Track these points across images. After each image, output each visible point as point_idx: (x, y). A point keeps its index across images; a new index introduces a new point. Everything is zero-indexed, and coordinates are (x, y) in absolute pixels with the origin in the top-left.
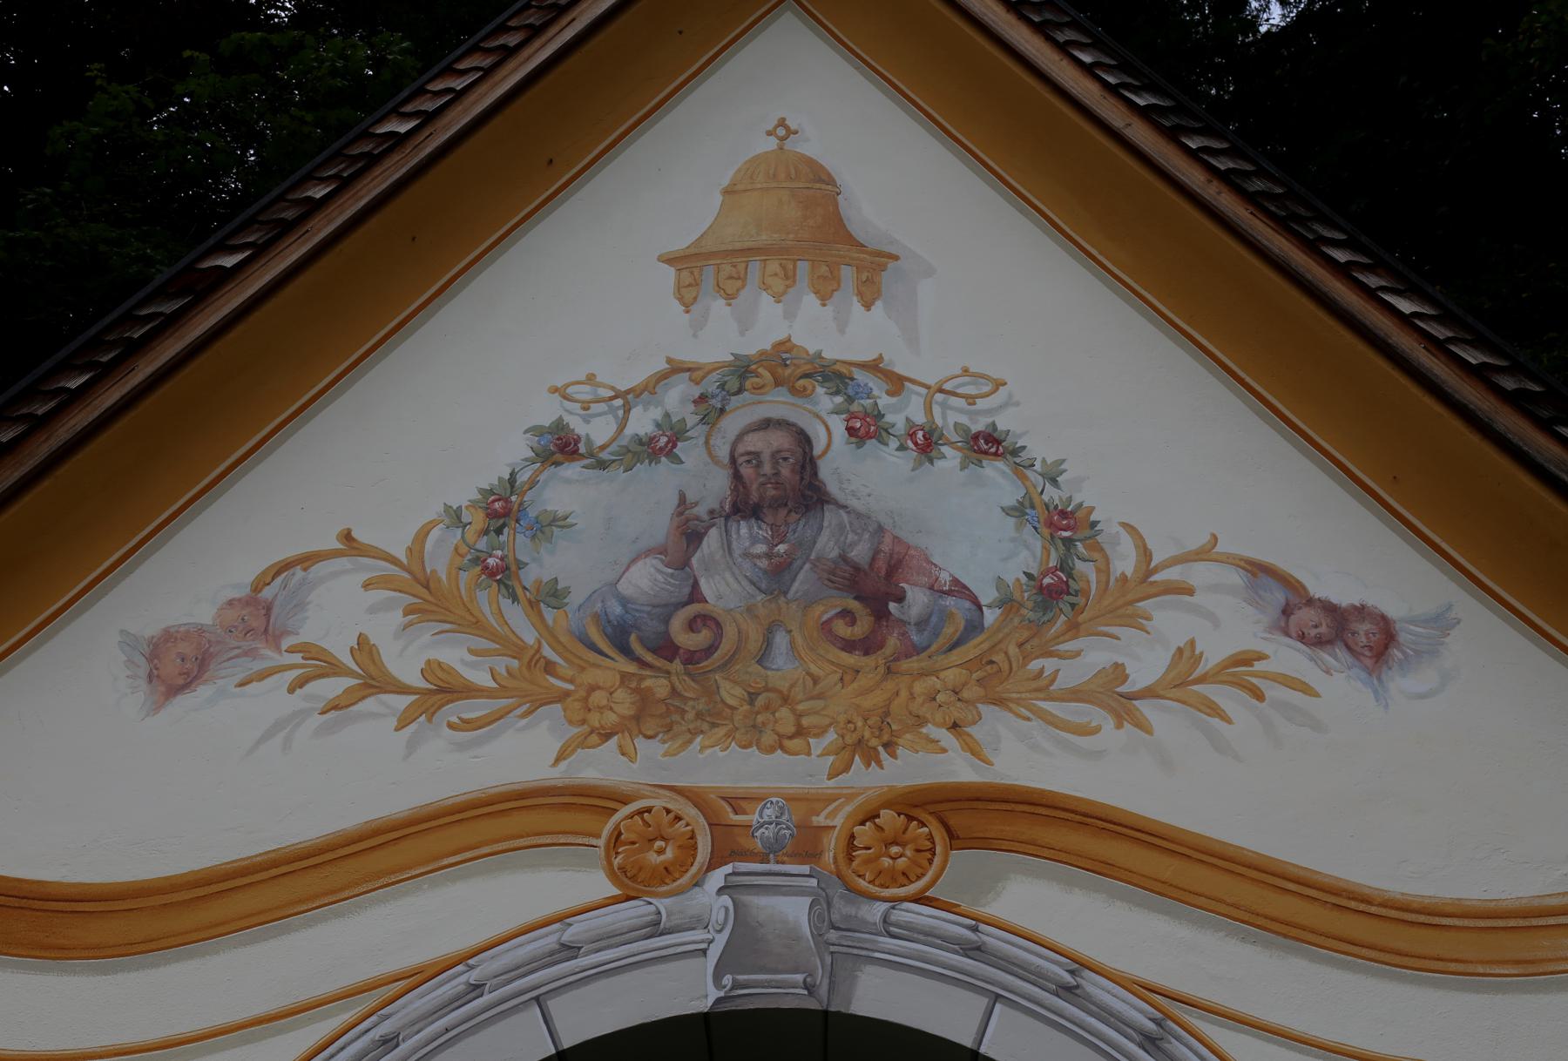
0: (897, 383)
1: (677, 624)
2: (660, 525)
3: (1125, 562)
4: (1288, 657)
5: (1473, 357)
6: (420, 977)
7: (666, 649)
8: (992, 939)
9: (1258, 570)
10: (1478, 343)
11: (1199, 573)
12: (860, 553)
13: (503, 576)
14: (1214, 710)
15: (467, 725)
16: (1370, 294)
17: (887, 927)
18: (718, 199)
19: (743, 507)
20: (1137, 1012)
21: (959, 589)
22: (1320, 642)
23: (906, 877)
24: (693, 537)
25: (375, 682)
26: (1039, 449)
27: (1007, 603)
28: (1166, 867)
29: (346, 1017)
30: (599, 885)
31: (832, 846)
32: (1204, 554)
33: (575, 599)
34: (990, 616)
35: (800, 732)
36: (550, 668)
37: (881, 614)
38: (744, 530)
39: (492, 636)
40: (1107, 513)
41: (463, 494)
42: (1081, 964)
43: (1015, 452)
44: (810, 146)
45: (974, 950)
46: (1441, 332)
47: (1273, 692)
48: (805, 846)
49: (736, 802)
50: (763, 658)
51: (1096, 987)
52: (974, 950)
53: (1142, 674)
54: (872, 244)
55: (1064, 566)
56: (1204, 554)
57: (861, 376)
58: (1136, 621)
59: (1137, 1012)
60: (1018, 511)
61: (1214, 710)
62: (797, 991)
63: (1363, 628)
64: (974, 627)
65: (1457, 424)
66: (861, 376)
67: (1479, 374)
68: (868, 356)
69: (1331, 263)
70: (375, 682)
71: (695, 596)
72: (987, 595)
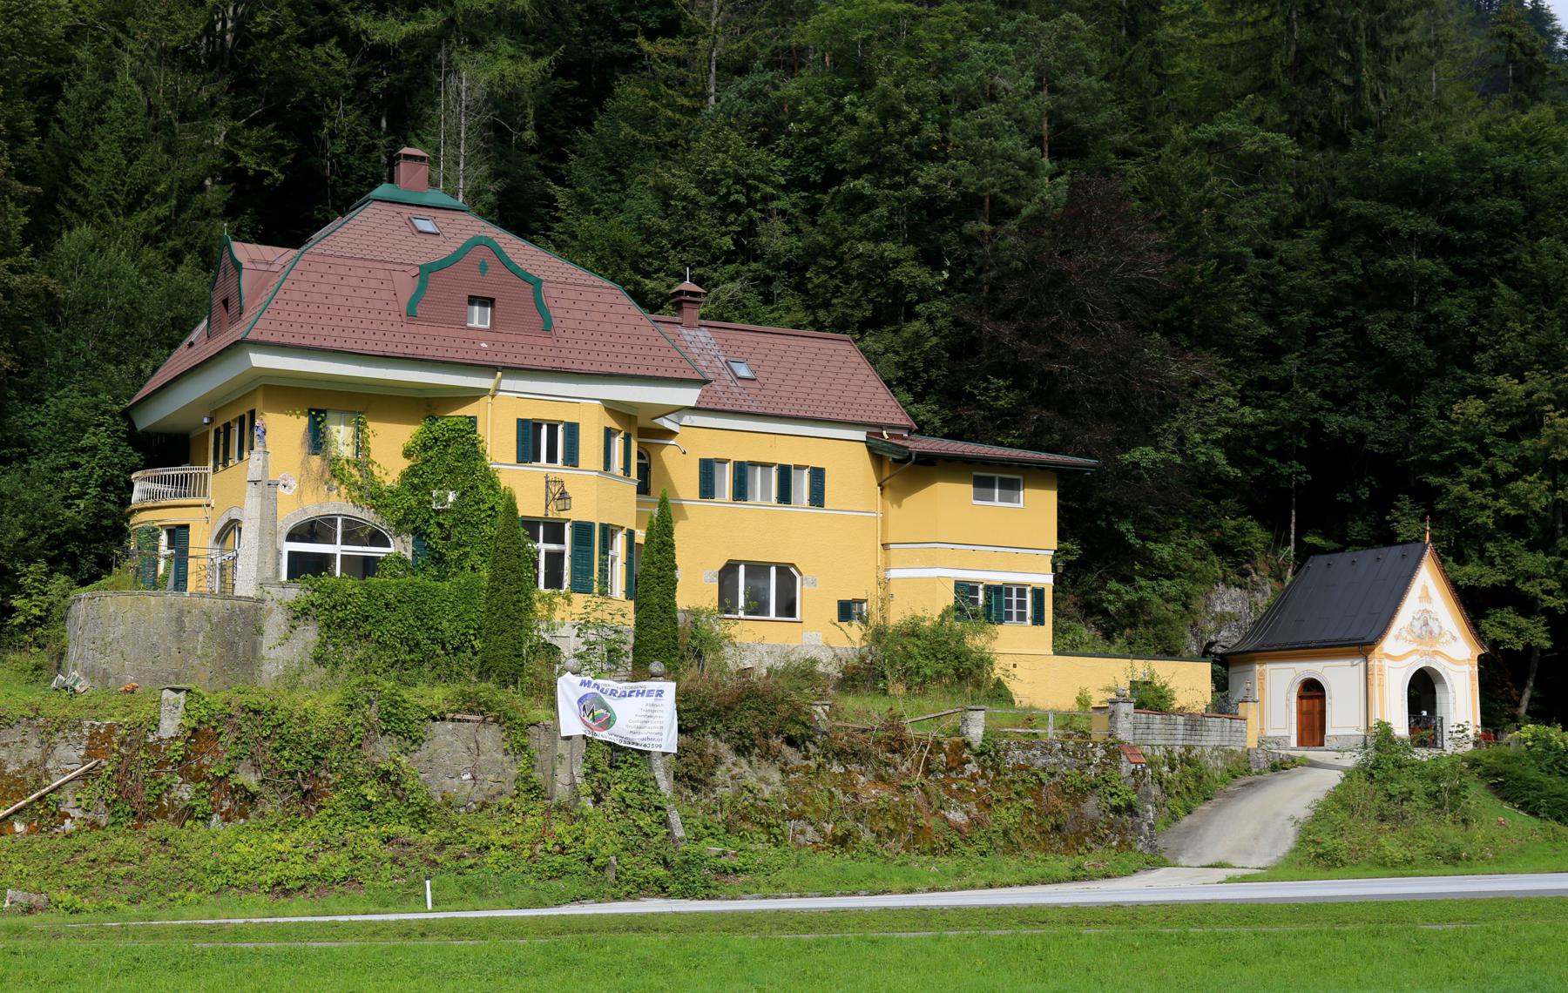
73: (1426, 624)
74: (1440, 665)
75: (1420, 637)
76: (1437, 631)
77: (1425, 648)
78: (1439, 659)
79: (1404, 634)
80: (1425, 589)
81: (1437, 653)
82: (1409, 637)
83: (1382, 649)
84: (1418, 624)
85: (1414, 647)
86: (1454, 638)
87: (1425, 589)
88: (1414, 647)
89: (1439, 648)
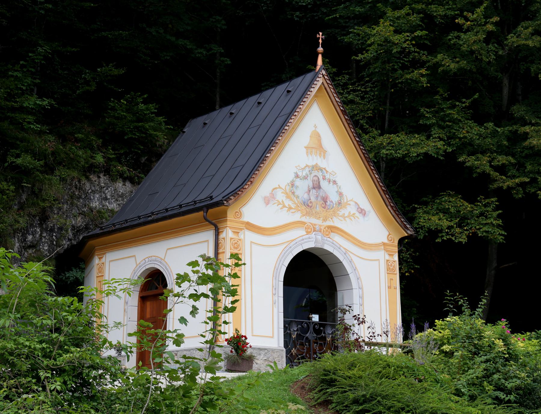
0: (327, 172)
1: (309, 202)
2: (306, 189)
3: (345, 201)
4: (357, 214)
5: (381, 184)
6: (292, 241)
7: (308, 206)
8: (334, 243)
9: (356, 203)
10: (382, 183)
11: (352, 203)
12: (324, 196)
13: (293, 193)
14: (351, 220)
15: (292, 213)
16: (373, 173)
17: (327, 240)
18: (309, 138)
19: (314, 188)
20: (344, 251)
21: (332, 202)
22: (360, 213)
23: (328, 235)
24: (310, 191)
25: (284, 206)
26: (339, 184)
27: (336, 204)
28: (349, 238)
29: (287, 244)
30: (304, 233)
31: (322, 231)
32: (352, 200)
33: (300, 198)
34: (334, 205)
35: (319, 218)
36: (299, 206)
37: (326, 204)
38: (314, 191)
39: (293, 201)
40: (344, 194)
41: (289, 182)
42: (341, 246)
43: (337, 184)
44: (318, 130)
45: (333, 243)
46: (379, 180)
47: (356, 218)
48: (320, 231)
49: (315, 225)
50: (316, 208)
51: (342, 248)
52: (333, 243)
53: (346, 215)
54: (325, 149)
55: (340, 200)
56: (352, 200)
57: (323, 170)
58: (346, 208)
59: (344, 251)
60: (337, 192)
61: (351, 220)
62: (304, 237)
63: (363, 212)
64: (333, 206)
65: (377, 191)
66: (323, 170)
67: (381, 186)
68: (324, 167)
69: (371, 168)
70: (284, 206)
71: (310, 199)
72: (334, 203)
73: (317, 186)
74: (339, 248)
75: (307, 204)
76: (334, 198)
77: (314, 221)
78: (337, 238)
79: (280, 196)
80: (316, 136)
81: (333, 229)
82: (287, 203)
83: (239, 214)
84: (303, 186)
85: (297, 217)
86: (362, 212)
87: (316, 136)
88: (297, 217)
89: (337, 223)
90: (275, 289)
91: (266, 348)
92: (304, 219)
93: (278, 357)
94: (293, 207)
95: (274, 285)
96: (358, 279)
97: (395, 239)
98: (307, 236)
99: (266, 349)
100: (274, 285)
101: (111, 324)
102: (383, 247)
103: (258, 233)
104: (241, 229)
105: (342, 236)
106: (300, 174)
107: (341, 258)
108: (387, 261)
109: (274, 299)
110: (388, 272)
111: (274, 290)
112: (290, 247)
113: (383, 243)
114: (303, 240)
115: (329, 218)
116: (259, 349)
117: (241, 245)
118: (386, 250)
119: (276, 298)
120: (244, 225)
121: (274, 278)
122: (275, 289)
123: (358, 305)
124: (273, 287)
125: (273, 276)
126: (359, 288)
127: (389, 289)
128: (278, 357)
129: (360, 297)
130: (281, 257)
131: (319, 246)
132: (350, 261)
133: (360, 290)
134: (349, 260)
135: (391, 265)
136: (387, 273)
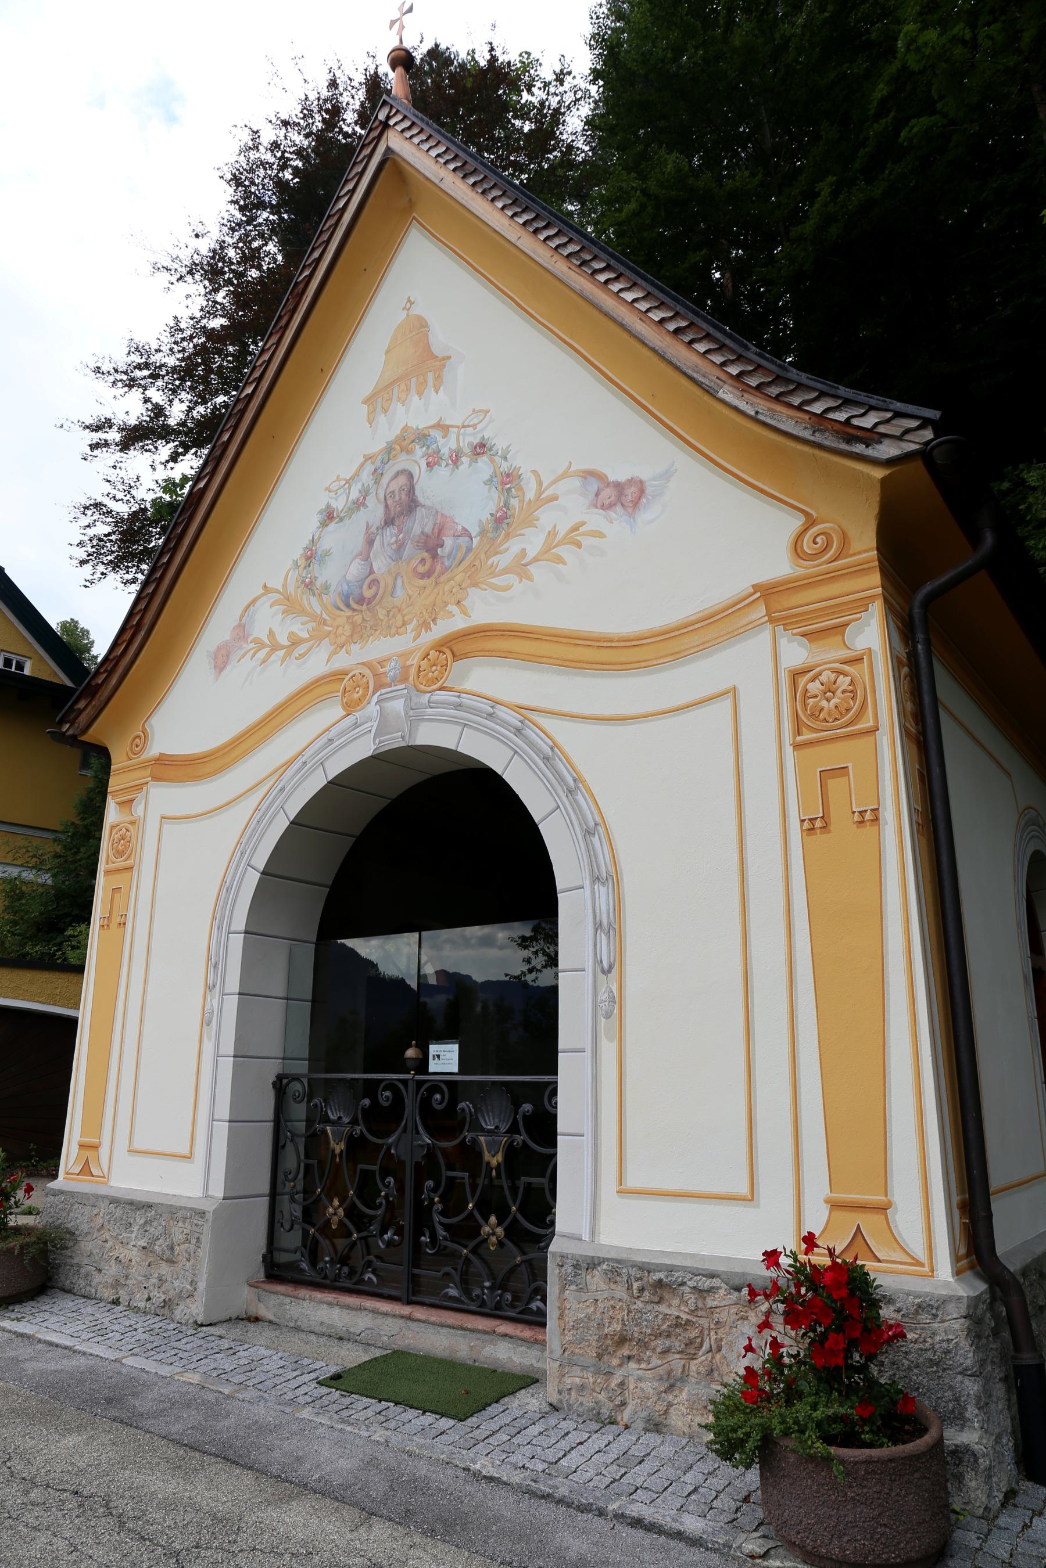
8: (466, 700)
20: (513, 718)
21: (466, 532)
51: (502, 712)
52: (458, 706)
59: (513, 718)
83: (144, 738)
90: (216, 966)
91: (151, 1200)
92: (342, 661)
93: (187, 1241)
94: (304, 635)
95: (213, 952)
96: (589, 833)
97: (852, 532)
98: (350, 720)
99: (150, 1206)
100: (213, 952)
101: (149, 406)
102: (761, 611)
103: (678, 656)
104: (139, 787)
105: (508, 655)
106: (339, 504)
107: (316, 783)
108: (796, 675)
109: (207, 1007)
110: (807, 736)
111: (211, 970)
112: (282, 790)
113: (756, 588)
114: (331, 741)
115: (446, 604)
116: (131, 1203)
117: (133, 840)
118: (779, 620)
119: (215, 1002)
120: (148, 772)
121: (216, 924)
122: (216, 966)
123: (589, 975)
124: (209, 958)
125: (214, 918)
126: (596, 879)
127: (819, 837)
128: (187, 1241)
129: (598, 927)
130: (244, 840)
131: (394, 741)
132: (546, 759)
133: (602, 891)
134: (538, 751)
135: (830, 690)
136: (797, 746)
